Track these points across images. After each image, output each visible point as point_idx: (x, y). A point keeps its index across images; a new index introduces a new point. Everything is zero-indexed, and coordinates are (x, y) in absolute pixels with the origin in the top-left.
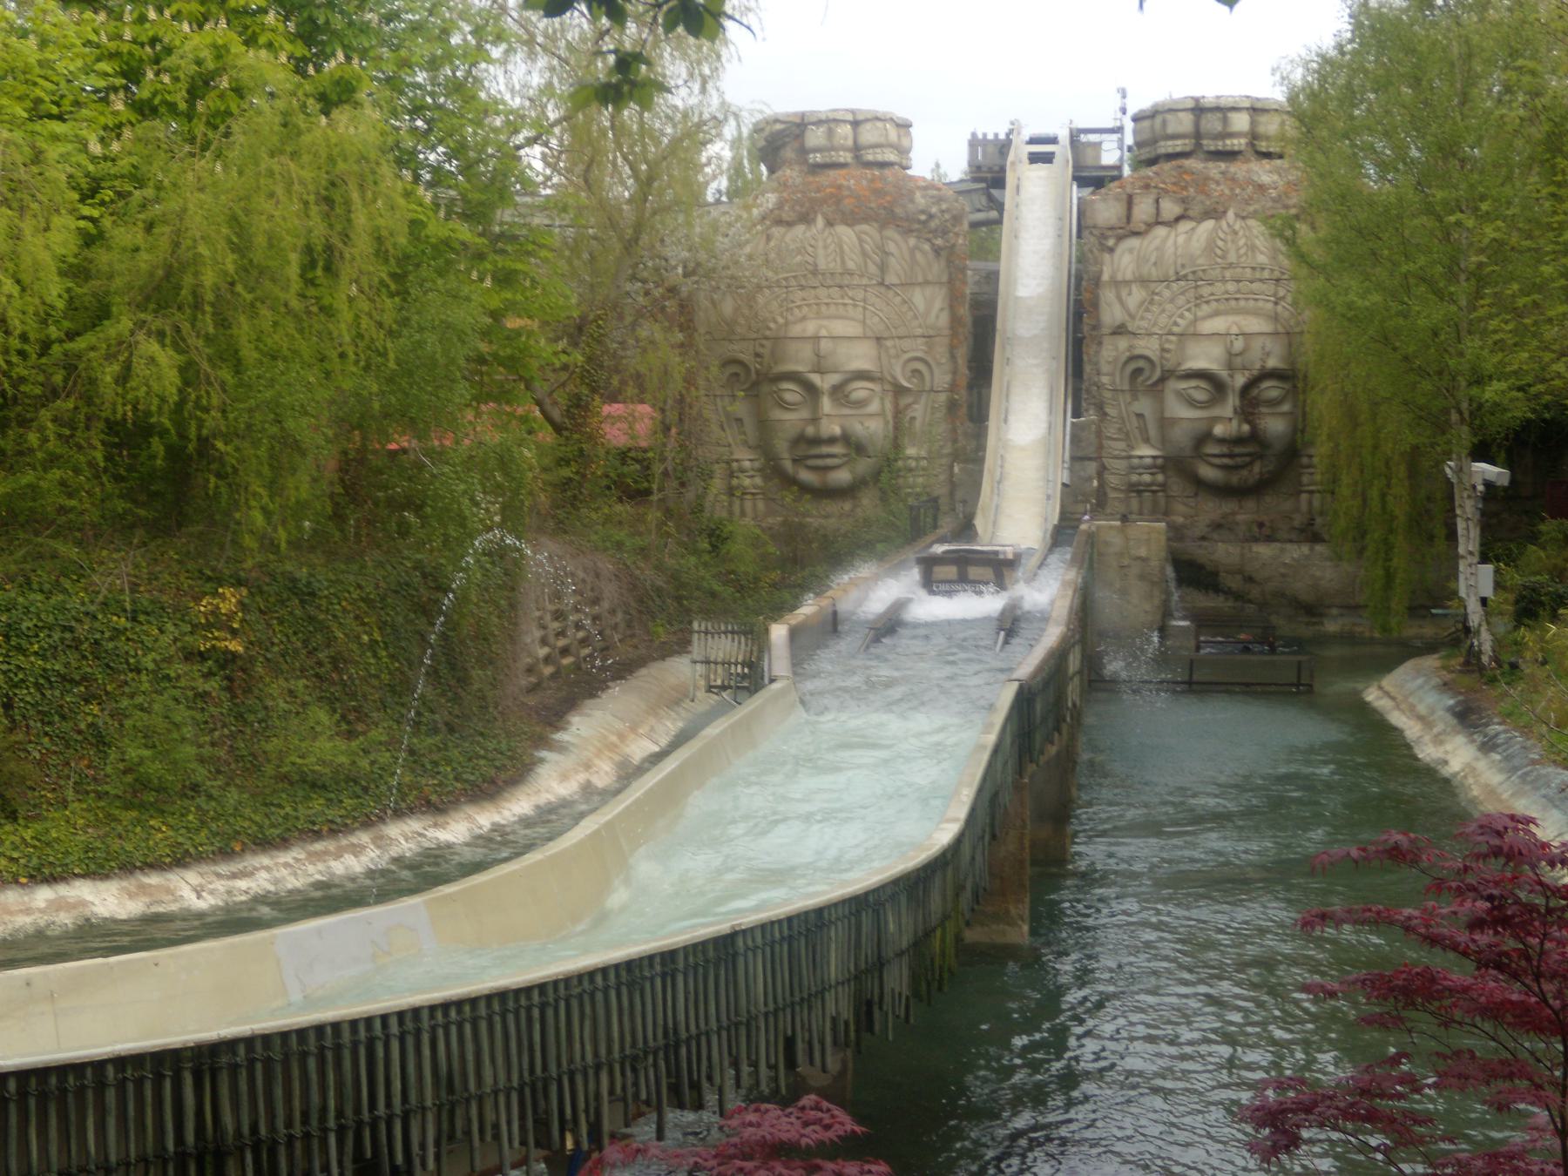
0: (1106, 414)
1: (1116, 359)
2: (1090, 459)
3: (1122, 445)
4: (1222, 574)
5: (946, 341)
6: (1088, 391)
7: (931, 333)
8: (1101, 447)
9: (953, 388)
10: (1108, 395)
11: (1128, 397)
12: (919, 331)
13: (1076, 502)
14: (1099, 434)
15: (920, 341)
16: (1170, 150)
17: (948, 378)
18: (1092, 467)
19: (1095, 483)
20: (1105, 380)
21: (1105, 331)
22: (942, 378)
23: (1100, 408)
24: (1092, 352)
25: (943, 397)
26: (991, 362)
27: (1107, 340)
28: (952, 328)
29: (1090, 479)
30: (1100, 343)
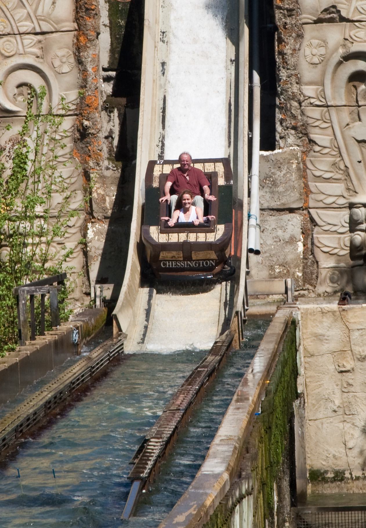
0: (312, 142)
1: (324, 60)
2: (291, 210)
3: (338, 188)
4: (131, 311)
5: (69, 38)
6: (284, 109)
7: (46, 27)
8: (307, 191)
9: (82, 109)
10: (314, 113)
11: (345, 115)
12: (26, 26)
13: (273, 277)
14: (303, 172)
15: (30, 40)
16: (61, 484)
17: (73, 96)
18: (294, 223)
19: (301, 248)
20: (309, 91)
21: (306, 17)
22: (64, 92)
23: (303, 131)
24: (288, 50)
25: (67, 124)
26: (136, 150)
27: (309, 31)
28: (77, 20)
29: (292, 240)
30: (300, 36)
